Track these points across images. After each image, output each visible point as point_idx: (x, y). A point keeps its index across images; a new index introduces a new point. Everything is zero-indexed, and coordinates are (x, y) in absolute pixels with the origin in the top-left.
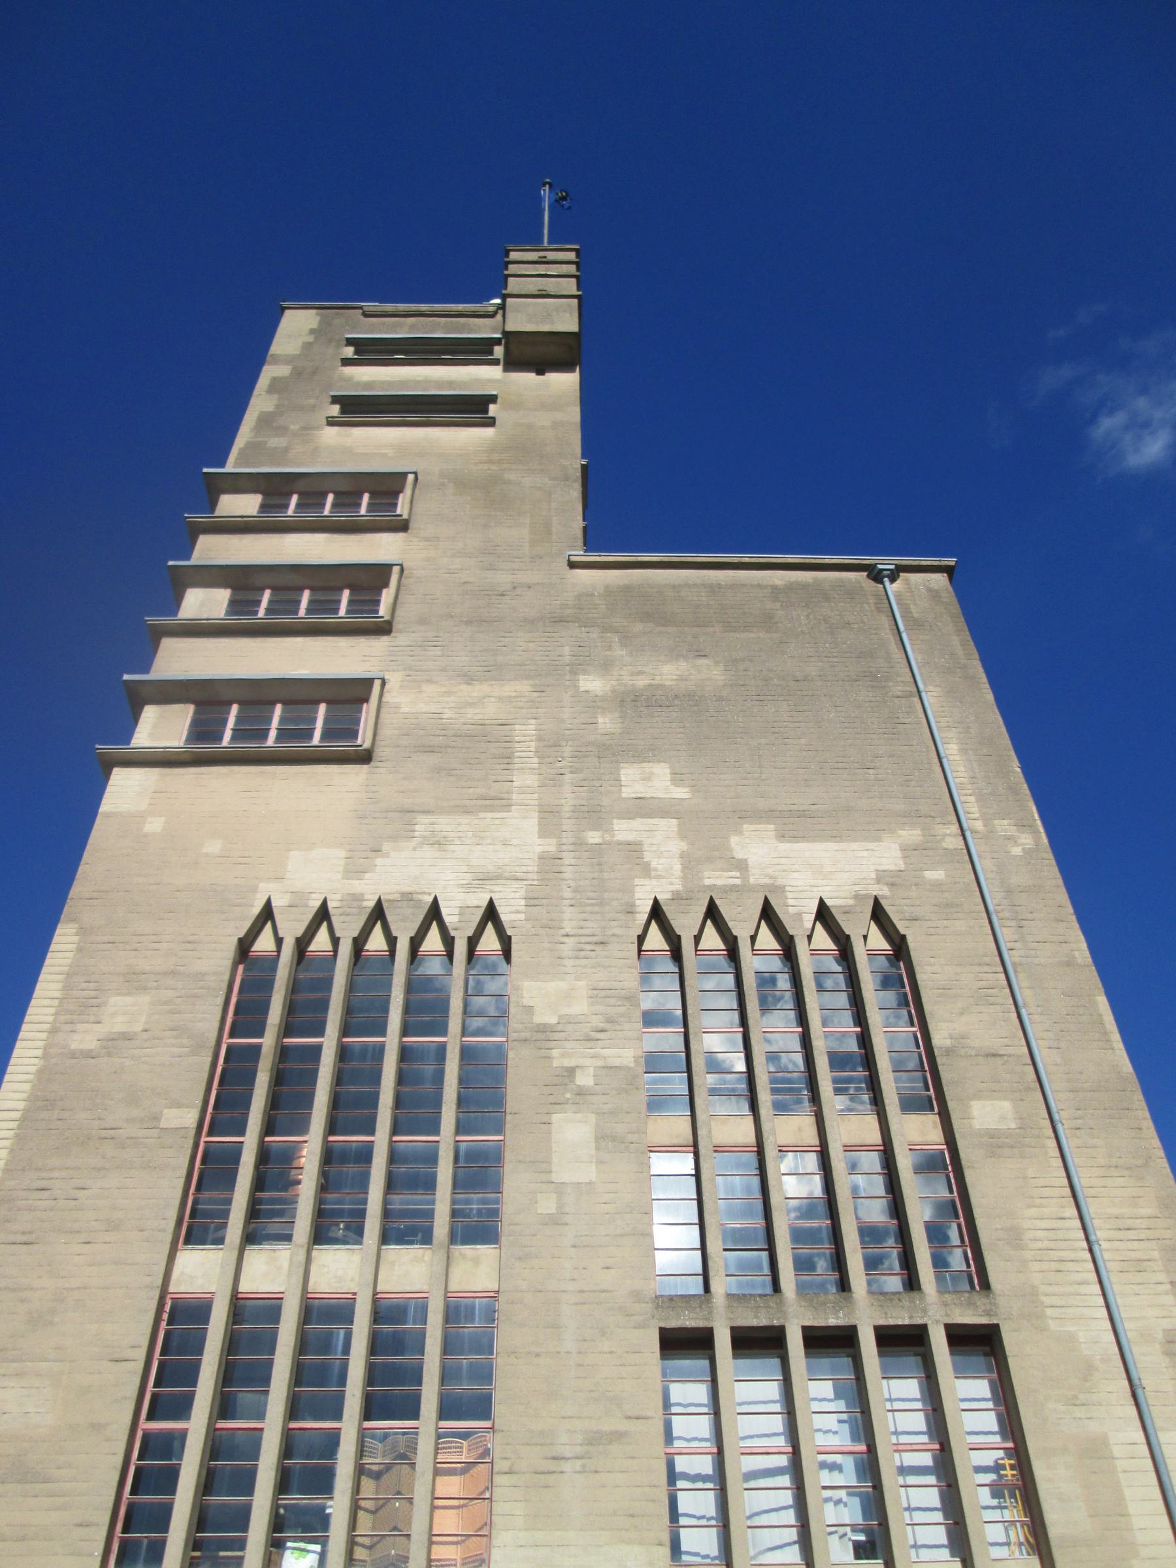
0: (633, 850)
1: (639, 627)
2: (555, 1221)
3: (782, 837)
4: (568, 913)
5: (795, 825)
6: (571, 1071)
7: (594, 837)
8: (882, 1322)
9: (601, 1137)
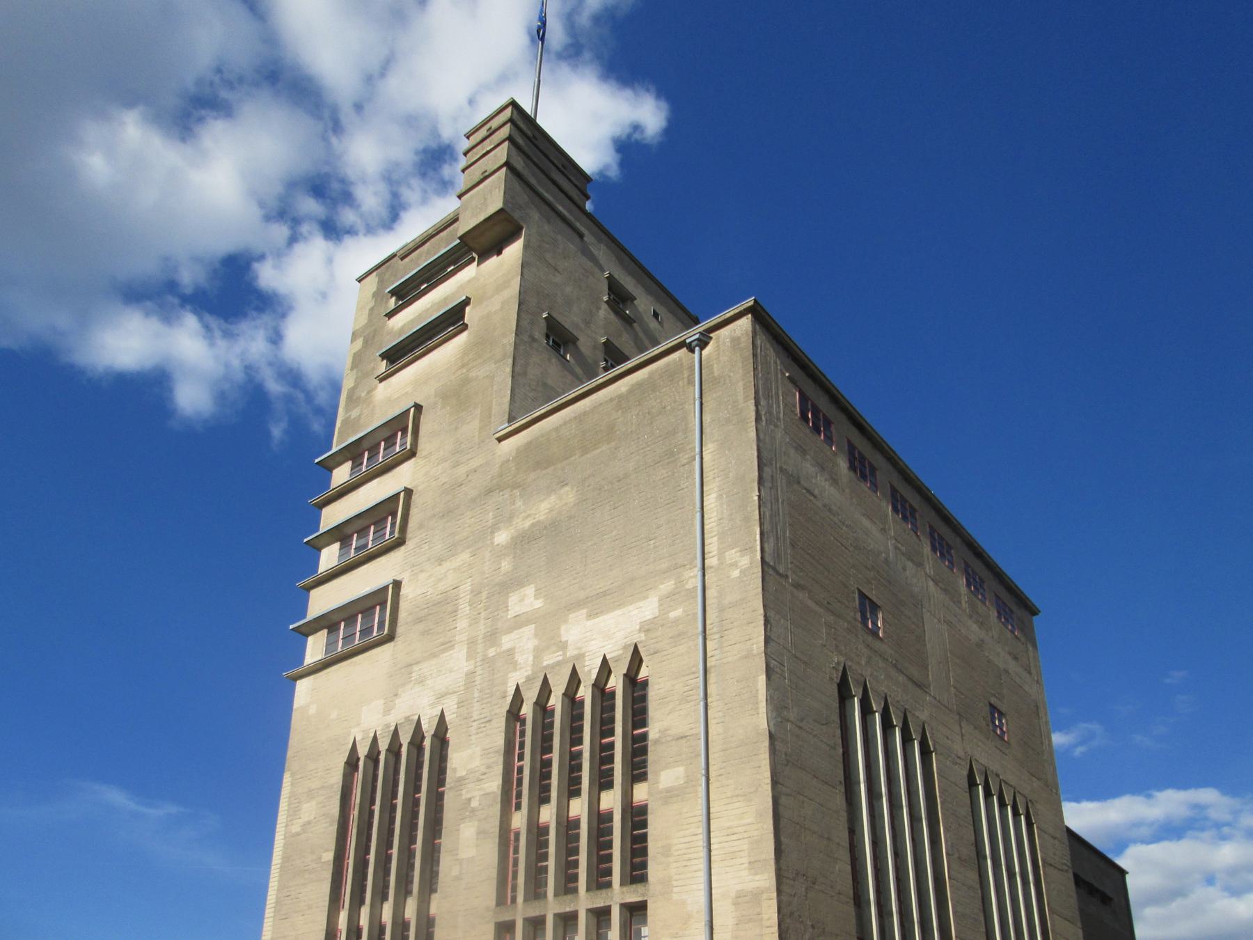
0: (511, 652)
1: (532, 476)
2: (458, 878)
3: (590, 616)
4: (476, 706)
5: (597, 603)
6: (469, 800)
7: (491, 652)
8: (590, 906)
9: (478, 833)
